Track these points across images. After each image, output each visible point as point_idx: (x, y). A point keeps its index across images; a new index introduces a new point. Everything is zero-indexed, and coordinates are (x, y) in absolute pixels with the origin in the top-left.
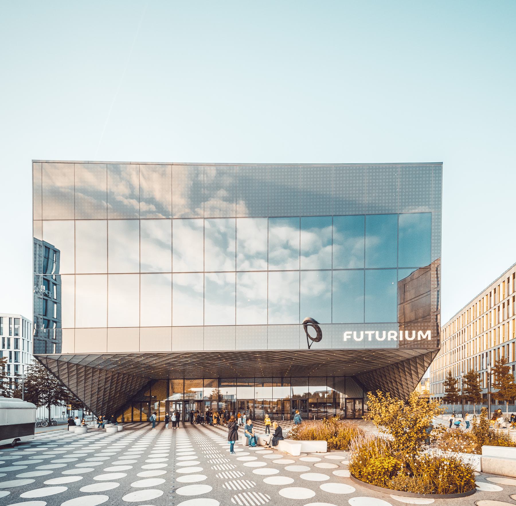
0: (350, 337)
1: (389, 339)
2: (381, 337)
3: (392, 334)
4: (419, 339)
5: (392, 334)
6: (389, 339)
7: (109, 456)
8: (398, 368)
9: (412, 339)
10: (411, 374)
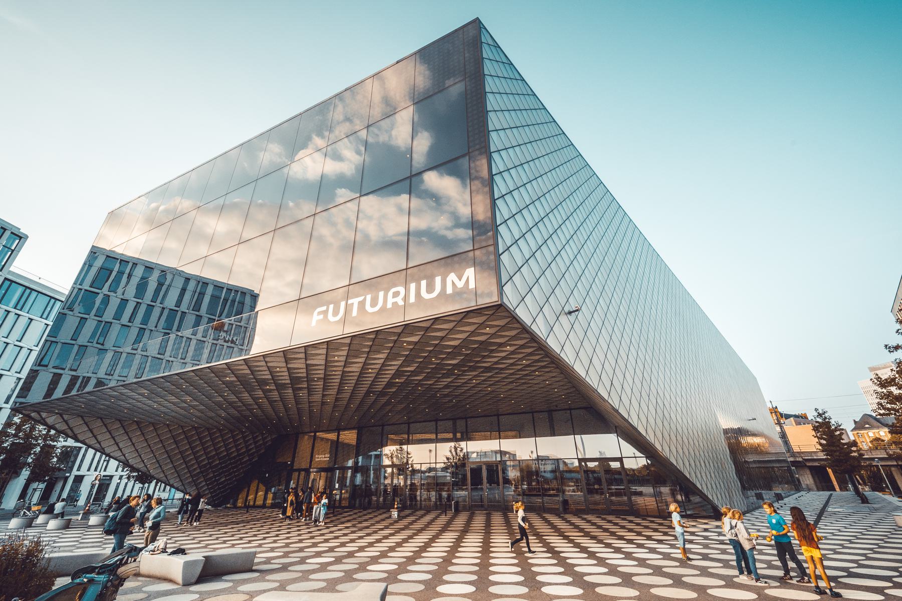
1: (389, 306)
5: (396, 294)
6: (389, 306)
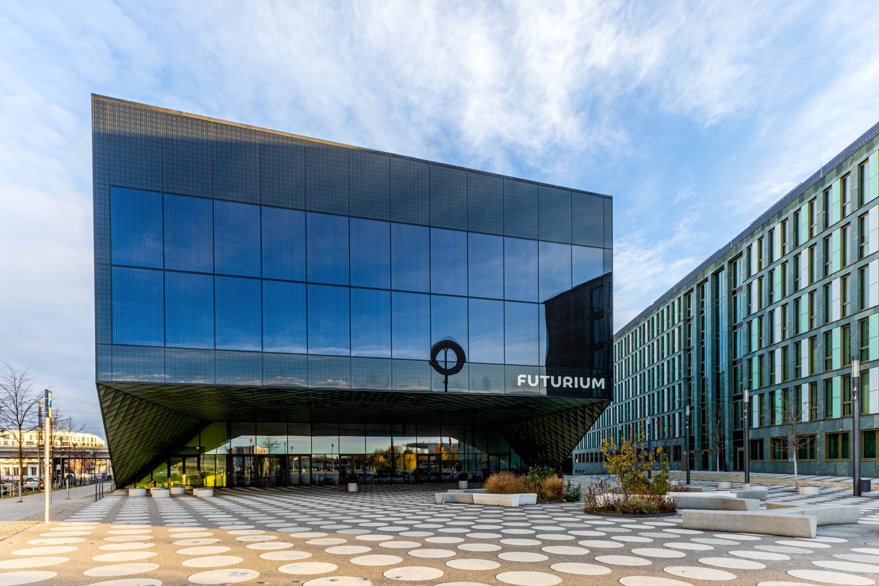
0: (524, 381)
1: (565, 386)
2: (556, 382)
3: (568, 381)
4: (593, 387)
5: (568, 381)
6: (565, 386)
7: (683, 551)
8: (561, 417)
9: (586, 387)
10: (576, 425)
